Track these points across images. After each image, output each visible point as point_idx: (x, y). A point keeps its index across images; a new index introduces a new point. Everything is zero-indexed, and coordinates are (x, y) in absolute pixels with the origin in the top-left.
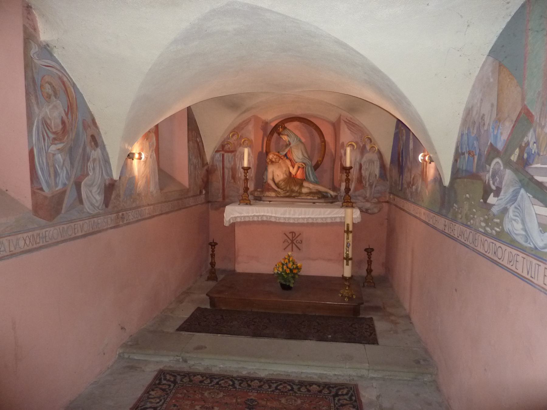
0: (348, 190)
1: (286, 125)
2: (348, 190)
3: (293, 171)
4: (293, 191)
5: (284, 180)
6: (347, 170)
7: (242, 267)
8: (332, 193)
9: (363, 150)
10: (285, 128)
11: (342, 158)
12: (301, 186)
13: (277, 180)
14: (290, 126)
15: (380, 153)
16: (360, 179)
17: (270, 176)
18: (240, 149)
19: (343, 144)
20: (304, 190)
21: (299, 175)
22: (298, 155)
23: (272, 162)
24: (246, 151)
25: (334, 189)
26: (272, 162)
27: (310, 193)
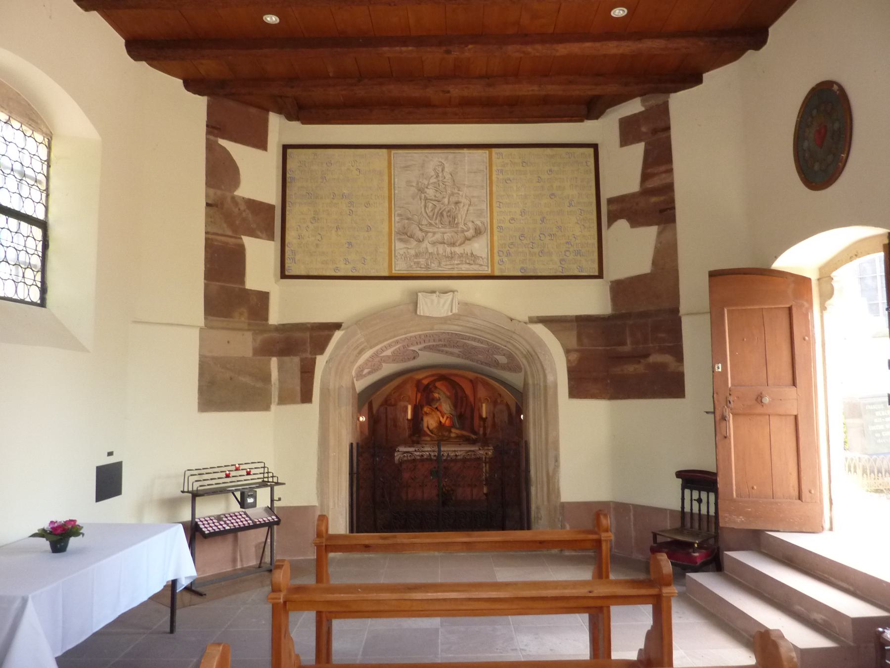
0: (485, 434)
1: (638, 149)
2: (485, 434)
3: (443, 421)
4: (444, 436)
5: (436, 428)
6: (484, 420)
7: (331, 532)
8: (474, 437)
9: (495, 403)
10: (436, 388)
11: (480, 410)
12: (450, 432)
13: (431, 427)
14: (438, 384)
15: (507, 405)
16: (494, 425)
17: (425, 425)
18: (402, 404)
19: (480, 400)
20: (453, 435)
21: (448, 423)
22: (446, 407)
23: (426, 414)
24: (410, 407)
25: (475, 433)
26: (426, 414)
27: (458, 437)
